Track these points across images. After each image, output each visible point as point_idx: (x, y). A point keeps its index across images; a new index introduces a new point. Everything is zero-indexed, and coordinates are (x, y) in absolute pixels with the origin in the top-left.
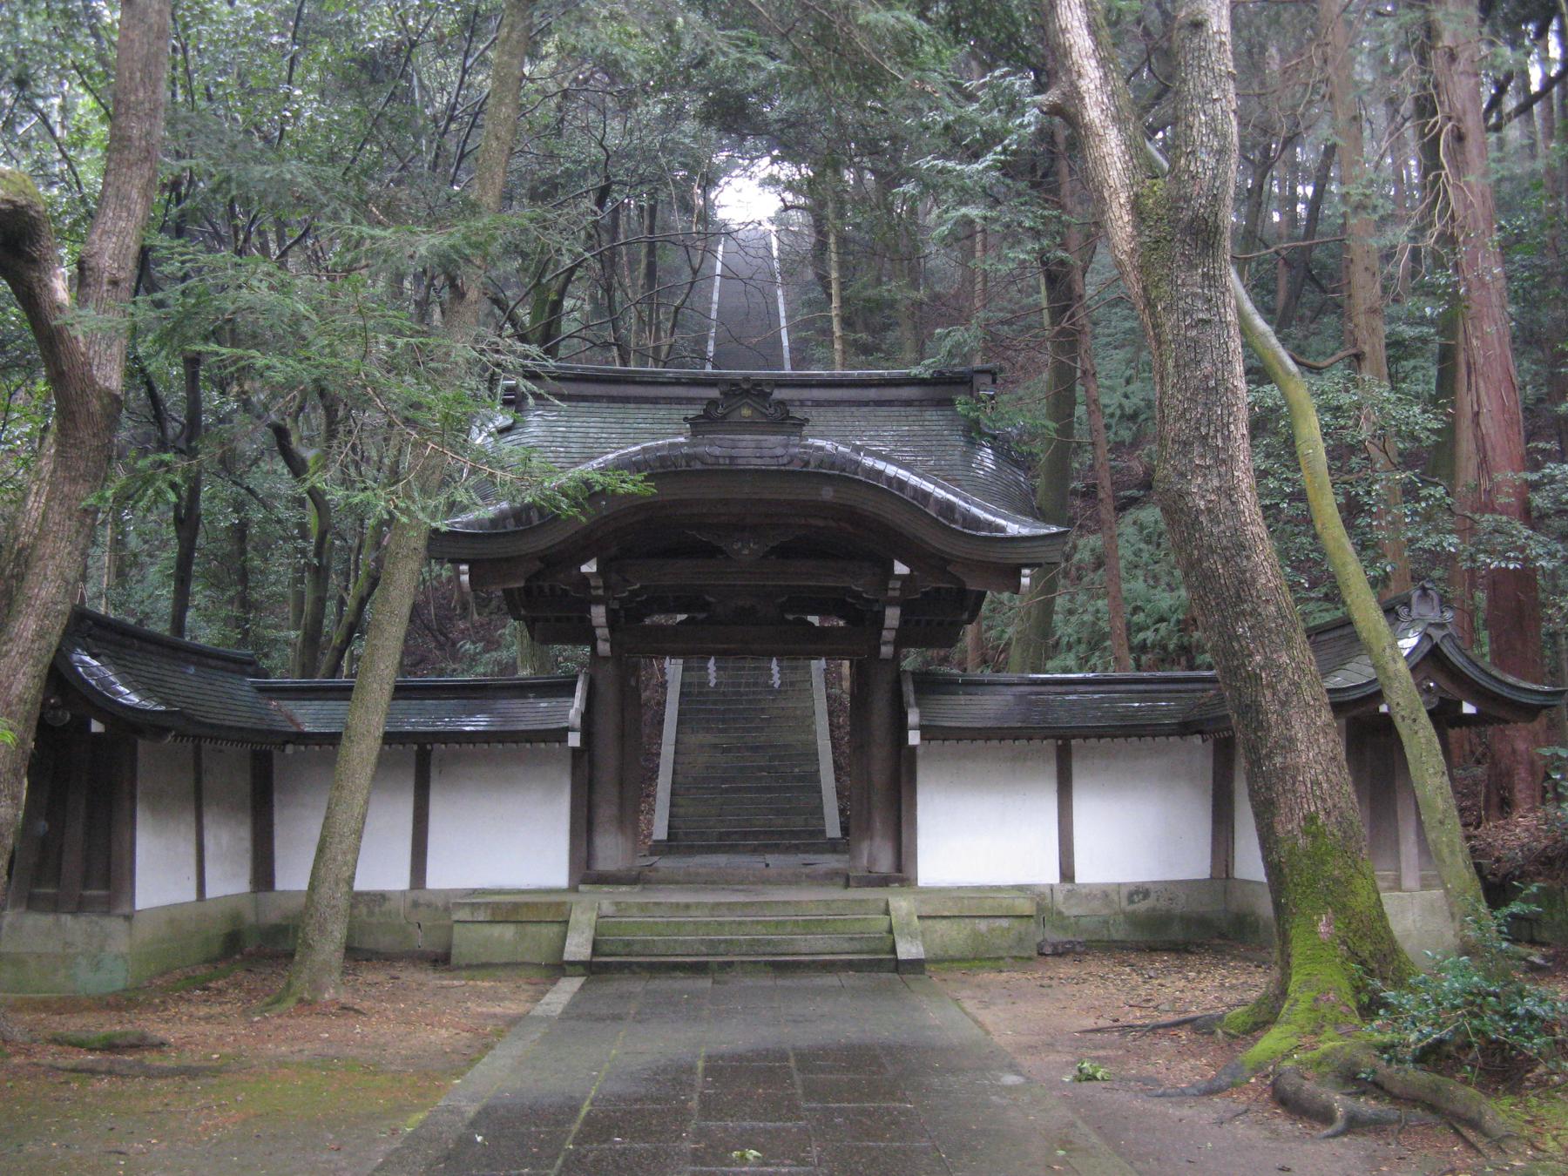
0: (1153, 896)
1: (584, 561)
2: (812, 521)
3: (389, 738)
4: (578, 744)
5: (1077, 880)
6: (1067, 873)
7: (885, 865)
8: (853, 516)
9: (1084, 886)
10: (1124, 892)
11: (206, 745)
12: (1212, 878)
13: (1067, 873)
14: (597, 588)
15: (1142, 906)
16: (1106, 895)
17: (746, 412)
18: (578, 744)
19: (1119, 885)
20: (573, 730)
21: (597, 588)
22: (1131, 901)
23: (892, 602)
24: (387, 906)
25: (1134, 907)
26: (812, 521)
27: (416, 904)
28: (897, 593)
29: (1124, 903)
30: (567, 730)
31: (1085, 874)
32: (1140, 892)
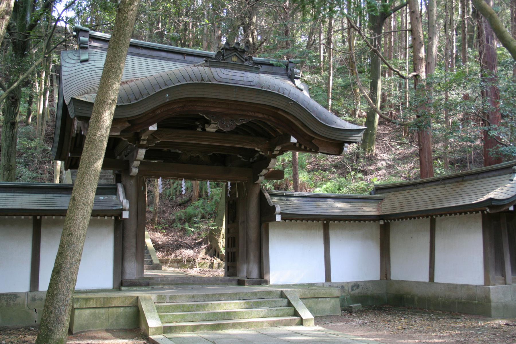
0: (361, 287)
1: (151, 124)
2: (257, 114)
3: (95, 214)
4: (127, 217)
5: (332, 281)
6: (328, 277)
7: (255, 274)
8: (274, 112)
9: (335, 283)
10: (350, 286)
11: (438, 219)
12: (381, 279)
13: (328, 277)
14: (144, 140)
15: (357, 292)
16: (342, 287)
17: (234, 59)
18: (127, 217)
19: (348, 283)
20: (125, 210)
21: (144, 140)
22: (353, 290)
23: (142, 147)
24: (18, 300)
25: (354, 292)
26: (257, 114)
27: (34, 299)
28: (145, 142)
29: (350, 290)
30: (122, 210)
31: (335, 278)
32: (356, 285)
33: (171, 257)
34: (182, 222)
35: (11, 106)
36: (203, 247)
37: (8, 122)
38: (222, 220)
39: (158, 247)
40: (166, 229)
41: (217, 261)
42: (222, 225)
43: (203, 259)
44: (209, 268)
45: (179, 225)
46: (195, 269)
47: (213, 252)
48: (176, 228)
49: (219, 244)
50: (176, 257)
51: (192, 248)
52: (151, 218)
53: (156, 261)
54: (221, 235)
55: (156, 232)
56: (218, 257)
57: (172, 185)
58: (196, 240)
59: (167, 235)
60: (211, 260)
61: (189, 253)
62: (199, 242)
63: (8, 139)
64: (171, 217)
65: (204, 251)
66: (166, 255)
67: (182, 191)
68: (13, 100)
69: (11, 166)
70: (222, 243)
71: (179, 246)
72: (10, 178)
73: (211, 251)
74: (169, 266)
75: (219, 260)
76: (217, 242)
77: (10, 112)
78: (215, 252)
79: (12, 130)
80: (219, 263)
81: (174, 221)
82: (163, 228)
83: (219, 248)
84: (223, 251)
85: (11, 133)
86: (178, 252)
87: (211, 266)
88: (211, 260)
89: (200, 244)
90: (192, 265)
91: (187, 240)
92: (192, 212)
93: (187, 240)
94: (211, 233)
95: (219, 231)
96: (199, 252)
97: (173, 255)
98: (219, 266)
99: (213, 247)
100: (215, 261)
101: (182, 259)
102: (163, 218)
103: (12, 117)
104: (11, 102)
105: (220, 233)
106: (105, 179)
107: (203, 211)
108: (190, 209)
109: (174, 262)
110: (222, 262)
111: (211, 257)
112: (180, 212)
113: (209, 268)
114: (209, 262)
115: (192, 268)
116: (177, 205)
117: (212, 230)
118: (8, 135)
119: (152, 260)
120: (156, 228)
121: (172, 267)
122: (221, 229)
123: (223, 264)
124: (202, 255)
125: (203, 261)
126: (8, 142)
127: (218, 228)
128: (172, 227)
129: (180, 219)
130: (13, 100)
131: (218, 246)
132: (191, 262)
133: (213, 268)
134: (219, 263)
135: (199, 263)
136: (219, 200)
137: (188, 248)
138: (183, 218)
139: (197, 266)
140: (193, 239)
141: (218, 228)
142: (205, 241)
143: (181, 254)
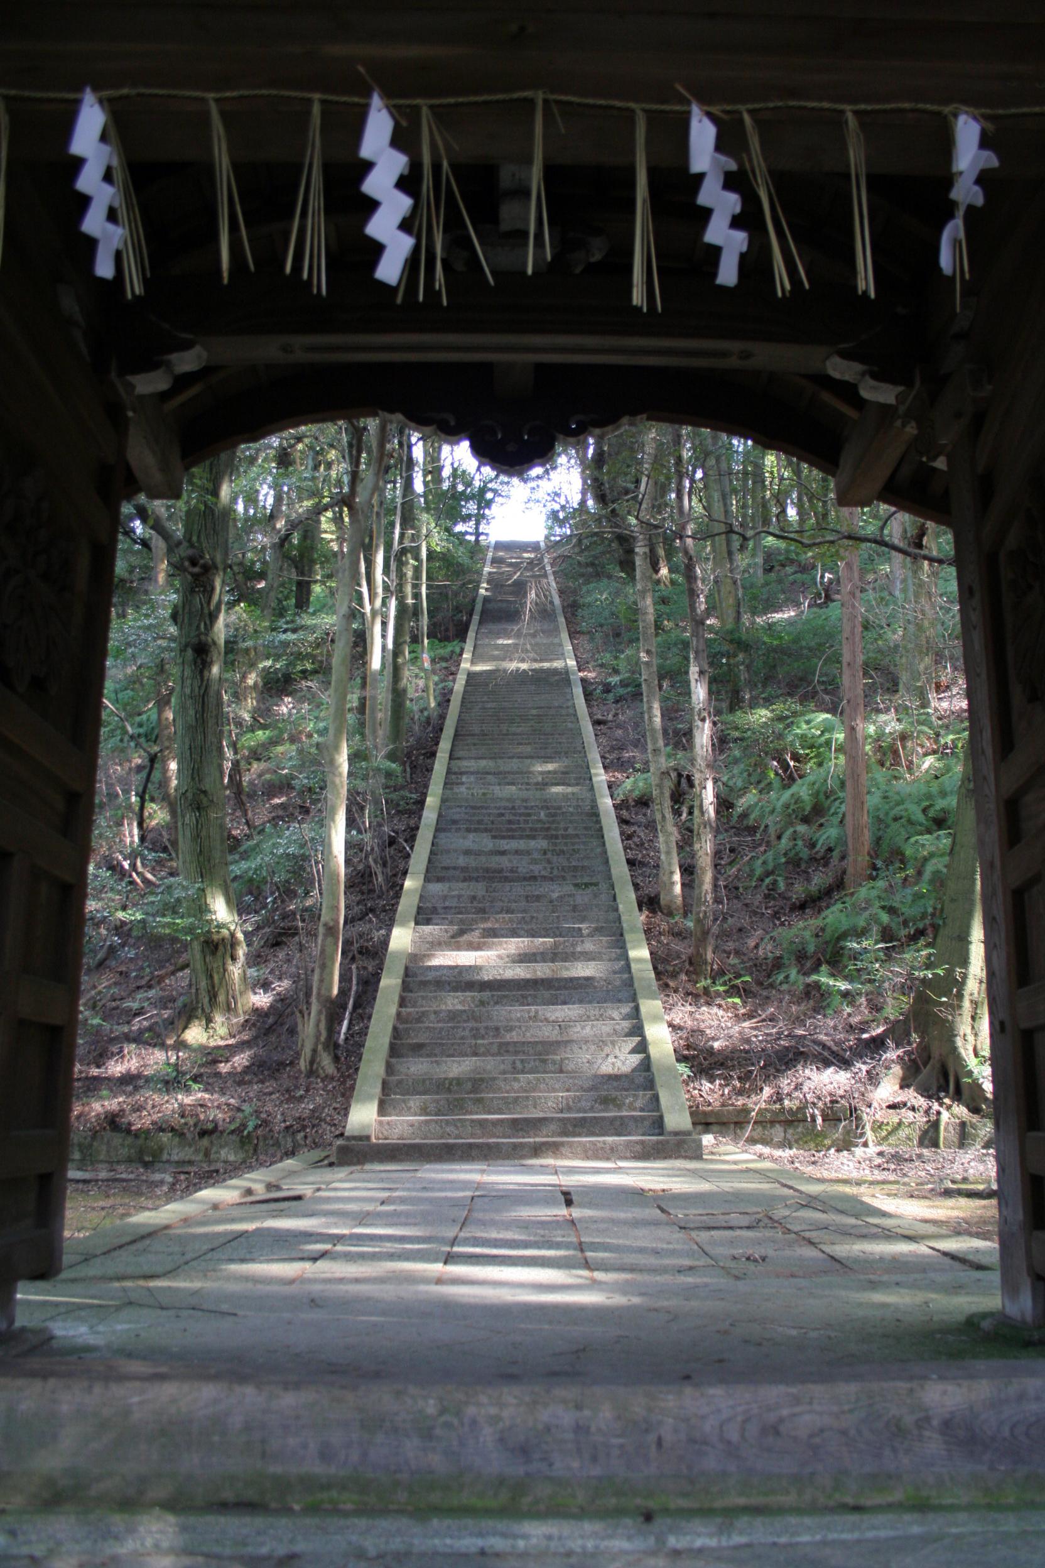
33: (761, 1100)
34: (808, 964)
35: (192, 591)
36: (892, 1054)
37: (186, 646)
38: (964, 940)
39: (700, 1059)
40: (744, 992)
41: (951, 1114)
42: (965, 962)
43: (893, 1107)
44: (921, 1144)
45: (793, 973)
46: (859, 1151)
47: (935, 1073)
48: (785, 987)
49: (959, 1042)
50: (780, 1100)
51: (845, 1063)
52: (690, 951)
53: (677, 1119)
54: (966, 1004)
55: (708, 1004)
56: (958, 1096)
57: (774, 842)
58: (863, 1031)
59: (749, 1016)
60: (927, 1112)
61: (829, 1081)
62: (873, 1039)
63: (189, 702)
64: (767, 950)
65: (897, 1070)
66: (740, 1092)
67: (377, 249)
68: (196, 570)
69: (205, 792)
70: (974, 1042)
71: (787, 1058)
72: (204, 833)
73: (925, 1071)
74: (752, 1141)
75: (961, 1110)
76: (949, 1033)
77: (190, 613)
78: (945, 1074)
79: (201, 672)
80: (963, 1124)
81: (778, 964)
82: (733, 991)
83: (958, 1058)
84: (983, 1074)
85: (196, 684)
86: (785, 1083)
87: (930, 1136)
88: (927, 1112)
89: (877, 1045)
90: (847, 1132)
91: (826, 1029)
92: (845, 924)
93: (826, 1029)
94: (922, 1000)
95: (953, 986)
96: (873, 1079)
97: (767, 1091)
98: (964, 1136)
99: (936, 1053)
100: (945, 1116)
101: (802, 1109)
102: (737, 953)
103: (198, 627)
104: (189, 577)
105: (960, 996)
106: (545, 837)
107: (885, 918)
108: (834, 916)
109: (772, 1123)
110: (975, 1119)
111: (929, 1097)
112: (802, 930)
113: (921, 1144)
114: (921, 1119)
115: (845, 1145)
116: (794, 908)
117: (924, 981)
118: (188, 691)
119: (661, 1117)
120: (706, 991)
121: (765, 1142)
122: (965, 976)
123: (986, 1129)
124: (888, 1090)
125: (893, 1117)
126: (192, 712)
127: (950, 972)
128: (772, 986)
129: (801, 956)
130: (196, 570)
131: (955, 1049)
132: (841, 1122)
133: (936, 1145)
134: (963, 1124)
135: (878, 1126)
136: (945, 870)
137: (827, 1064)
138: (811, 948)
139: (870, 1135)
140: (851, 1028)
141: (950, 972)
142: (898, 1032)
143: (798, 1087)
